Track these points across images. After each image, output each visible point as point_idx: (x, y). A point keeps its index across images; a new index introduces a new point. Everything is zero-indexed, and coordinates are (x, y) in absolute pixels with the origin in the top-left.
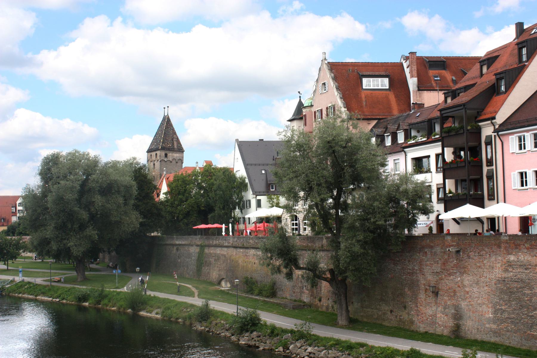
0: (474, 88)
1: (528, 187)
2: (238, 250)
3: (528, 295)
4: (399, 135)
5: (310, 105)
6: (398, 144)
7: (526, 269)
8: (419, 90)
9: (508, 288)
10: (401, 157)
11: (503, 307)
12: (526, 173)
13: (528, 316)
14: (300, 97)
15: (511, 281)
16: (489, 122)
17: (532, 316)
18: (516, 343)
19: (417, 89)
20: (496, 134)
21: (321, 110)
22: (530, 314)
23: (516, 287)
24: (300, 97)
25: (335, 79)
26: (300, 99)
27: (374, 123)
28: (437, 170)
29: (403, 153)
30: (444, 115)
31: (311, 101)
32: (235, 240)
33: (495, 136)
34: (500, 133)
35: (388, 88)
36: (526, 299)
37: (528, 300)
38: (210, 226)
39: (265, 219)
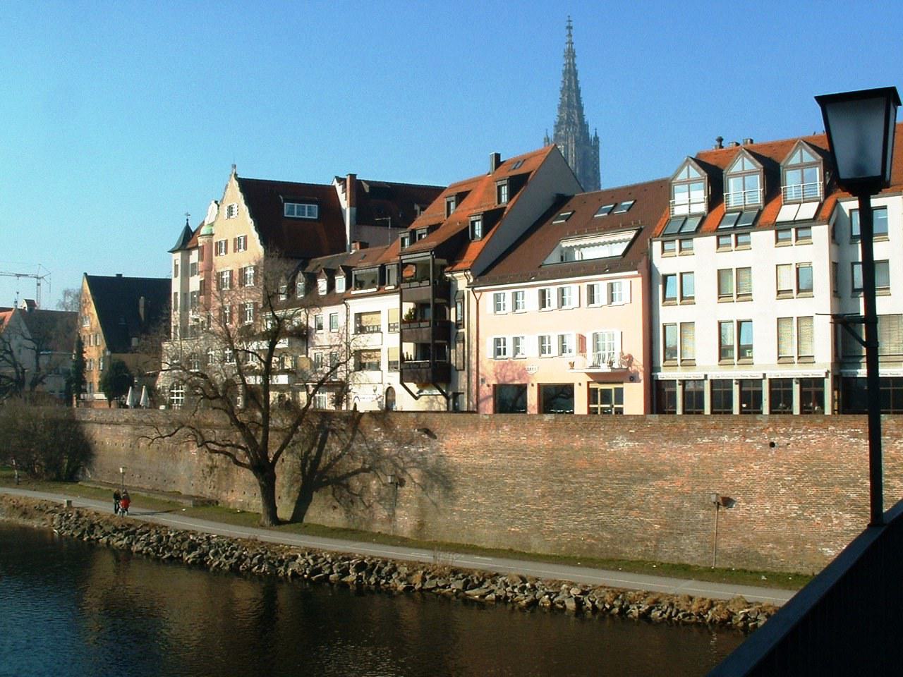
0: (438, 231)
1: (505, 357)
2: (105, 427)
3: (510, 485)
4: (337, 282)
5: (209, 233)
6: (335, 294)
7: (509, 455)
8: (357, 223)
9: (486, 477)
10: (339, 310)
11: (479, 500)
12: (504, 339)
13: (509, 509)
14: (187, 220)
15: (490, 469)
16: (462, 274)
17: (514, 509)
18: (441, 555)
19: (355, 222)
20: (470, 289)
21: (226, 242)
22: (512, 508)
23: (496, 476)
24: (187, 220)
25: (248, 202)
26: (187, 223)
27: (301, 261)
28: (389, 331)
29: (344, 305)
30: (404, 262)
31: (210, 228)
32: (100, 414)
33: (468, 292)
34: (476, 289)
35: (316, 218)
36: (508, 489)
37: (509, 491)
38: (899, 388)
39: (820, 389)
